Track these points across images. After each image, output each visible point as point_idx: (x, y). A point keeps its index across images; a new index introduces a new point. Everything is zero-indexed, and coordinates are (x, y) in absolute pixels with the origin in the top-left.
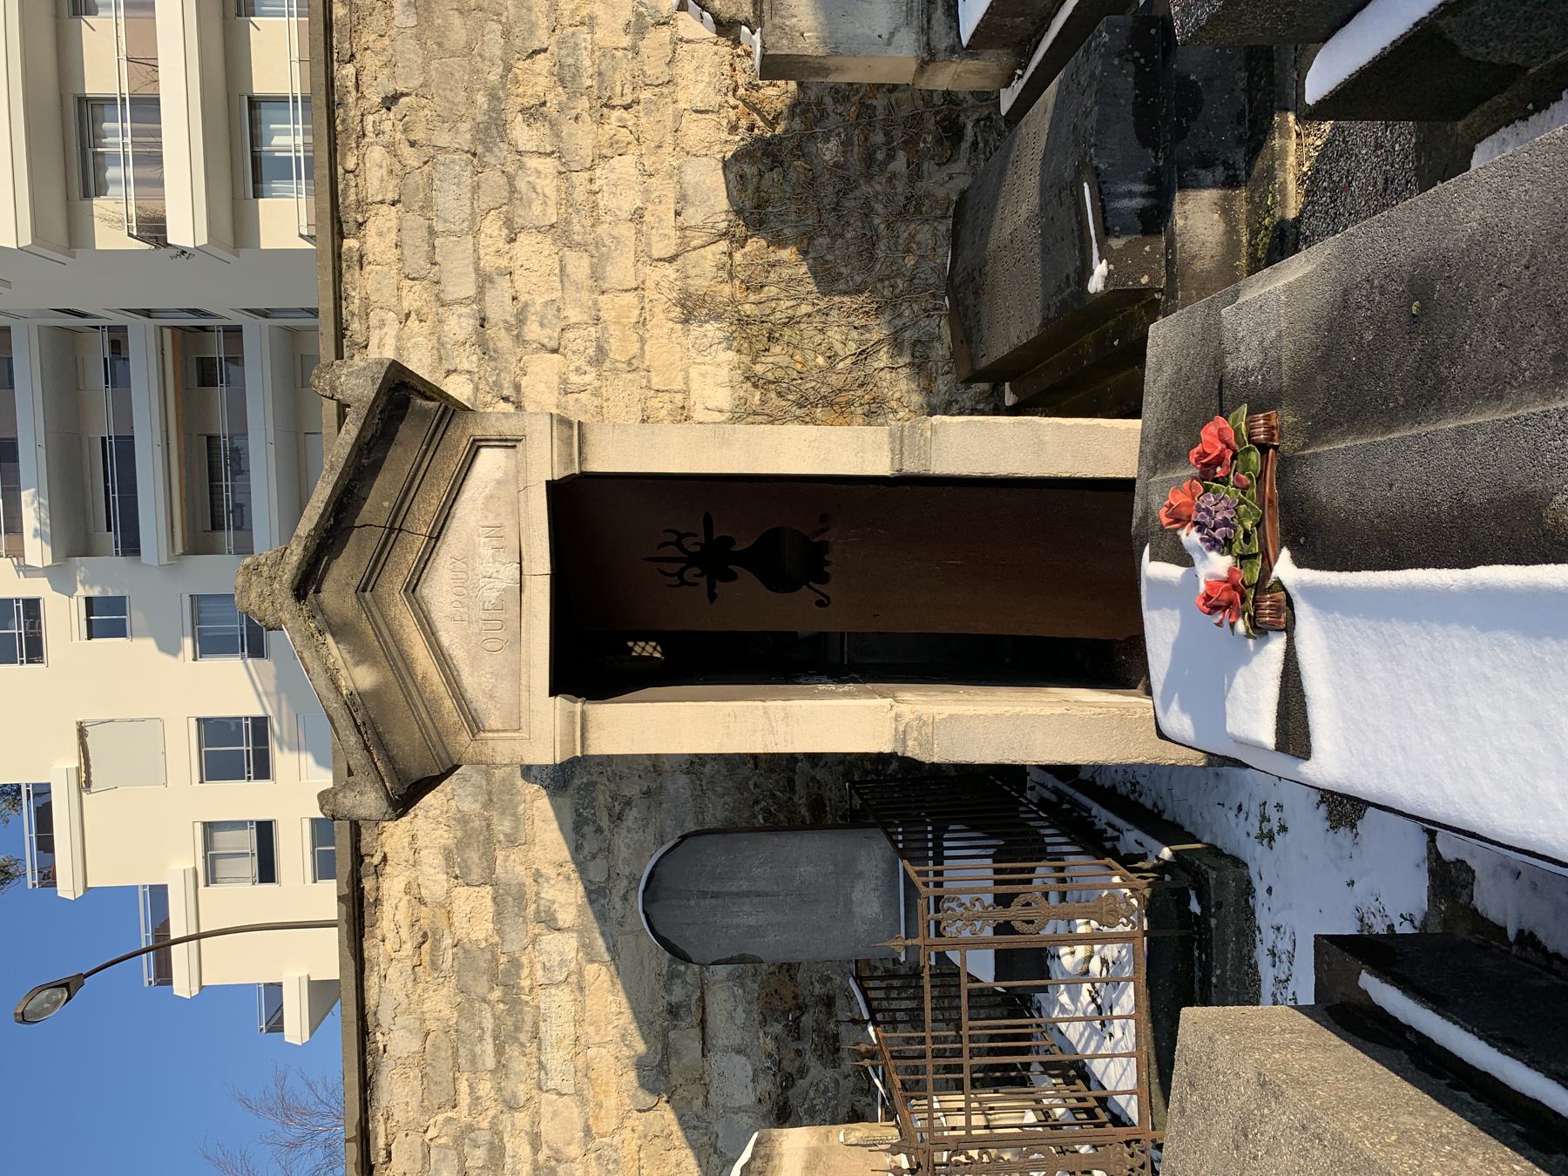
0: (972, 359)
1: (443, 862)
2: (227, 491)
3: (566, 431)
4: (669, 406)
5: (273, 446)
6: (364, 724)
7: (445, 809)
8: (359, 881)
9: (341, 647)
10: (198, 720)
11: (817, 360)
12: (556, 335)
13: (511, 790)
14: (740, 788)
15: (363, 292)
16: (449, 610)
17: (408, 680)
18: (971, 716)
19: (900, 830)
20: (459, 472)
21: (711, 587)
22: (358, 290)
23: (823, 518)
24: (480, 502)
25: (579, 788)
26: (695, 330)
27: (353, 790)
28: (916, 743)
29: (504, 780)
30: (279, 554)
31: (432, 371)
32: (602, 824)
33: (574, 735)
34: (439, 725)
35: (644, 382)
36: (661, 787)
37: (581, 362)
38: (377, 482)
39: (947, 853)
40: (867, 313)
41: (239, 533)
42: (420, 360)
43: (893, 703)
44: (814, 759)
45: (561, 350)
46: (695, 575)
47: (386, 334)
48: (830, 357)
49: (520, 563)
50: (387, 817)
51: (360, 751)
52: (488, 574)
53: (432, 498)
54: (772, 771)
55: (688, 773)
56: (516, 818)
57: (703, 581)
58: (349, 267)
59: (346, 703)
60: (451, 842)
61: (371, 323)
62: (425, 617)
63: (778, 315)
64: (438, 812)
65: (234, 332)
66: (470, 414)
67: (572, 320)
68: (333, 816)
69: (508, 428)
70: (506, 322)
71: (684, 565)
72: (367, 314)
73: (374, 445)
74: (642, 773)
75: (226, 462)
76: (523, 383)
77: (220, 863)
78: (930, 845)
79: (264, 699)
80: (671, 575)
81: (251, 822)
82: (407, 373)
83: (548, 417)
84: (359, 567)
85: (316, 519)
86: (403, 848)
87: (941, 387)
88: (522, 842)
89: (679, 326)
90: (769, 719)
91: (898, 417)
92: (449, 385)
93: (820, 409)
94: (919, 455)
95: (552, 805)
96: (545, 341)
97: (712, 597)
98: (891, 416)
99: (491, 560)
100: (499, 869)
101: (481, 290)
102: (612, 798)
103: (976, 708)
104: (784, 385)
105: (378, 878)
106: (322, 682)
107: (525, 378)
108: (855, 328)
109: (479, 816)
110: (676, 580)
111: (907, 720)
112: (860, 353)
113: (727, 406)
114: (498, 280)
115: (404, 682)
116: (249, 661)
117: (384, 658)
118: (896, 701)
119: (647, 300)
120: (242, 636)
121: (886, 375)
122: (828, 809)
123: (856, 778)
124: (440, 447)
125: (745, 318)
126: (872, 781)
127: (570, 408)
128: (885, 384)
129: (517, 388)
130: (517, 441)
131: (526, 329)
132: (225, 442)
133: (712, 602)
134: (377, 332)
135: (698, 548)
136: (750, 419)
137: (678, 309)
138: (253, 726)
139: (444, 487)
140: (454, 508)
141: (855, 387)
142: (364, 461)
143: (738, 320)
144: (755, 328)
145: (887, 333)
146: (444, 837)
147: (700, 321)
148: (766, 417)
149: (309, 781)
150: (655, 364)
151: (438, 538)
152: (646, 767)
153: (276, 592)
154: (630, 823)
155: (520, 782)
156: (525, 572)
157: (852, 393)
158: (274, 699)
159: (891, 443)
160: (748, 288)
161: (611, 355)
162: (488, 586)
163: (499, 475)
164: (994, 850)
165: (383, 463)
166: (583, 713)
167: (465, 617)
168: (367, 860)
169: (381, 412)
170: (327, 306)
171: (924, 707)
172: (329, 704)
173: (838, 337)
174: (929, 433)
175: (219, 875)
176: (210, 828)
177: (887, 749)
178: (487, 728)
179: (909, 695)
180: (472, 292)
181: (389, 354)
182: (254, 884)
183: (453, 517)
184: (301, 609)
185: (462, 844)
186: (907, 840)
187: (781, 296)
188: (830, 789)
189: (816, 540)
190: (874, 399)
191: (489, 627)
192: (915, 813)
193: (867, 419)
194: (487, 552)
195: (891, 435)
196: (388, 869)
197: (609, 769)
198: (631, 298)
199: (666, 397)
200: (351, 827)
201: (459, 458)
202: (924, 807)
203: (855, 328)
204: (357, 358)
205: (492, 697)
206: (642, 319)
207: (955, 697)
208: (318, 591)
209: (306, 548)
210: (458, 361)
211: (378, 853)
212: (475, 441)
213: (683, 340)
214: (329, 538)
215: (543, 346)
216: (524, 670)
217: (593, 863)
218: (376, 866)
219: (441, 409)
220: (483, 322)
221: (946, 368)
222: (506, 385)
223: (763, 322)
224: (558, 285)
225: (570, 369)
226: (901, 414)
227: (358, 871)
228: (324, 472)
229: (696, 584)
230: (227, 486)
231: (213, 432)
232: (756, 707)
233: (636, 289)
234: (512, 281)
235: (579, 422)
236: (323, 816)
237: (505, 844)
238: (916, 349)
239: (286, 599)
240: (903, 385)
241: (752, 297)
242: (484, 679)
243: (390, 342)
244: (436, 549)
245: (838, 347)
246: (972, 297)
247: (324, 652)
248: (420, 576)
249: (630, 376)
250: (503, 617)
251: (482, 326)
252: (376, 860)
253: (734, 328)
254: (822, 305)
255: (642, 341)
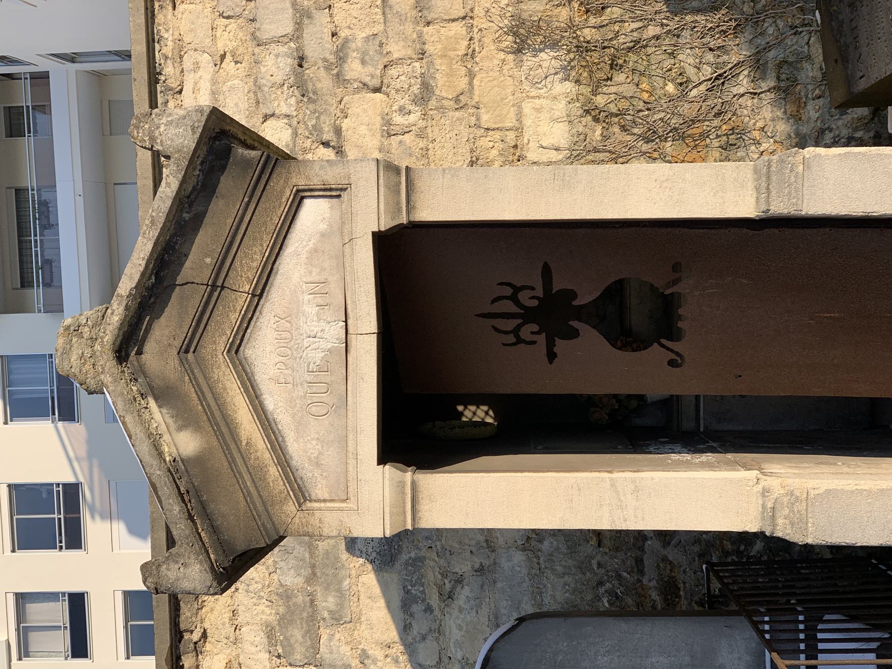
0: (849, 81)
1: (265, 640)
2: (36, 247)
3: (393, 178)
4: (500, 145)
5: (81, 199)
6: (188, 492)
7: (267, 583)
8: (179, 658)
9: (164, 411)
10: (9, 486)
11: (667, 88)
12: (378, 72)
13: (334, 563)
14: (583, 567)
15: (177, 33)
16: (273, 371)
17: (233, 446)
18: (852, 492)
19: (767, 619)
20: (282, 224)
21: (550, 345)
22: (171, 32)
23: (676, 267)
24: (304, 256)
25: (407, 564)
26: (529, 60)
27: (177, 562)
28: (787, 522)
29: (327, 553)
30: (100, 314)
31: (249, 117)
32: (432, 603)
33: (404, 507)
34: (265, 494)
35: (473, 120)
36: (495, 563)
37: (404, 100)
38: (198, 237)
39: (821, 646)
40: (725, 32)
41: (49, 290)
42: (236, 105)
43: (760, 476)
44: (665, 536)
45: (384, 88)
46: (532, 333)
47: (200, 78)
48: (681, 84)
49: (346, 322)
50: (212, 591)
51: (184, 522)
52: (312, 334)
53: (255, 253)
54: (617, 549)
55: (524, 550)
56: (341, 595)
57: (542, 339)
58: (161, 7)
59: (169, 471)
60: (273, 619)
61: (184, 66)
62: (249, 379)
63: (622, 39)
64: (260, 586)
65: (41, 79)
66: (293, 163)
67: (396, 55)
68: (156, 589)
69: (332, 176)
70: (325, 60)
71: (520, 321)
72: (181, 57)
73: (196, 198)
74: (474, 549)
75: (34, 216)
76: (344, 126)
77: (33, 636)
78: (802, 636)
79: (76, 464)
80: (506, 333)
81: (64, 594)
82: (228, 121)
83: (375, 163)
84: (181, 327)
85: (137, 277)
86: (224, 624)
87: (812, 113)
88: (348, 619)
89: (511, 57)
90: (617, 493)
91: (762, 149)
92: (267, 130)
93: (670, 143)
94: (789, 193)
95: (378, 581)
96: (367, 80)
97: (552, 356)
98: (753, 148)
99: (315, 318)
100: (323, 649)
101: (299, 26)
102: (442, 575)
103: (857, 482)
104: (628, 117)
105: (197, 655)
106: (145, 448)
107: (346, 121)
108: (711, 49)
109: (302, 590)
110: (511, 339)
111: (776, 495)
112: (716, 78)
113: (564, 143)
114: (317, 14)
115: (228, 448)
116: (60, 424)
117: (207, 423)
118: (763, 474)
119: (476, 30)
120: (53, 398)
121: (747, 101)
122: (682, 593)
123: (715, 559)
124: (263, 199)
125: (585, 45)
126: (733, 563)
127: (393, 151)
128: (745, 112)
129: (338, 131)
130: (341, 190)
131: (346, 67)
132: (33, 195)
133: (551, 362)
134: (192, 75)
135: (535, 303)
136: (590, 157)
137: (510, 38)
138: (64, 493)
139: (267, 241)
140: (277, 263)
141: (711, 115)
142: (186, 216)
143: (577, 47)
144: (595, 55)
145: (748, 54)
146: (266, 613)
147: (535, 50)
148: (608, 154)
149: (122, 551)
150: (485, 100)
151: (261, 296)
152: (478, 543)
153: (98, 354)
154: (461, 603)
155: (345, 556)
156: (350, 331)
157: (707, 123)
158: (85, 464)
159: (757, 180)
160: (587, 11)
161: (437, 92)
162: (313, 346)
163: (323, 227)
164: (878, 644)
165: (204, 216)
166: (414, 484)
167: (290, 379)
168: (186, 636)
169: (202, 163)
170: (139, 49)
171: (797, 480)
172: (152, 471)
173: (691, 60)
174: (801, 168)
175: (31, 648)
176: (22, 599)
177: (753, 528)
178: (313, 497)
179: (779, 466)
180: (289, 29)
181: (205, 101)
182: (66, 659)
183: (277, 272)
184: (123, 372)
185: (285, 621)
186: (776, 631)
187: (626, 17)
188: (685, 572)
189: (668, 292)
190: (733, 129)
191: (314, 390)
192: (784, 600)
193: (725, 153)
194: (311, 310)
195: (756, 171)
196: (208, 646)
197: (438, 543)
198: (458, 28)
199: (497, 135)
200: (170, 601)
201: (282, 210)
202: (795, 594)
203: (711, 49)
204: (171, 104)
205: (318, 465)
206: (470, 51)
207: (833, 469)
208: (139, 353)
209: (127, 308)
210: (276, 104)
211: (198, 629)
212: (298, 191)
213: (515, 72)
214: (150, 297)
215: (365, 85)
216: (351, 437)
217: (422, 645)
218: (196, 643)
219: (263, 159)
220: (301, 61)
221: (817, 92)
222: (326, 129)
223: (605, 48)
224: (380, 17)
225: (394, 108)
226: (764, 146)
227: (177, 648)
228: (145, 228)
229: (534, 343)
230: (36, 241)
231: (22, 185)
232: (603, 479)
233: (464, 18)
234: (331, 15)
235: (407, 167)
236: (145, 588)
237: (329, 622)
238: (782, 71)
239: (107, 361)
240: (767, 113)
241: (592, 21)
242: (309, 446)
243: (205, 86)
244: (259, 308)
245: (691, 72)
246: (848, 10)
247: (147, 416)
248: (243, 336)
249: (457, 114)
250: (328, 380)
251: (301, 66)
252: (196, 636)
253: (572, 56)
254: (673, 25)
255: (471, 75)
